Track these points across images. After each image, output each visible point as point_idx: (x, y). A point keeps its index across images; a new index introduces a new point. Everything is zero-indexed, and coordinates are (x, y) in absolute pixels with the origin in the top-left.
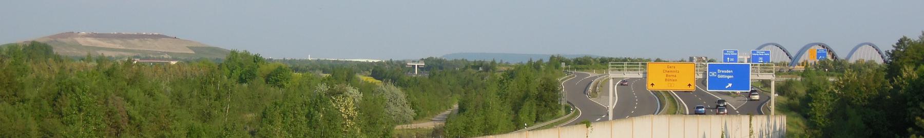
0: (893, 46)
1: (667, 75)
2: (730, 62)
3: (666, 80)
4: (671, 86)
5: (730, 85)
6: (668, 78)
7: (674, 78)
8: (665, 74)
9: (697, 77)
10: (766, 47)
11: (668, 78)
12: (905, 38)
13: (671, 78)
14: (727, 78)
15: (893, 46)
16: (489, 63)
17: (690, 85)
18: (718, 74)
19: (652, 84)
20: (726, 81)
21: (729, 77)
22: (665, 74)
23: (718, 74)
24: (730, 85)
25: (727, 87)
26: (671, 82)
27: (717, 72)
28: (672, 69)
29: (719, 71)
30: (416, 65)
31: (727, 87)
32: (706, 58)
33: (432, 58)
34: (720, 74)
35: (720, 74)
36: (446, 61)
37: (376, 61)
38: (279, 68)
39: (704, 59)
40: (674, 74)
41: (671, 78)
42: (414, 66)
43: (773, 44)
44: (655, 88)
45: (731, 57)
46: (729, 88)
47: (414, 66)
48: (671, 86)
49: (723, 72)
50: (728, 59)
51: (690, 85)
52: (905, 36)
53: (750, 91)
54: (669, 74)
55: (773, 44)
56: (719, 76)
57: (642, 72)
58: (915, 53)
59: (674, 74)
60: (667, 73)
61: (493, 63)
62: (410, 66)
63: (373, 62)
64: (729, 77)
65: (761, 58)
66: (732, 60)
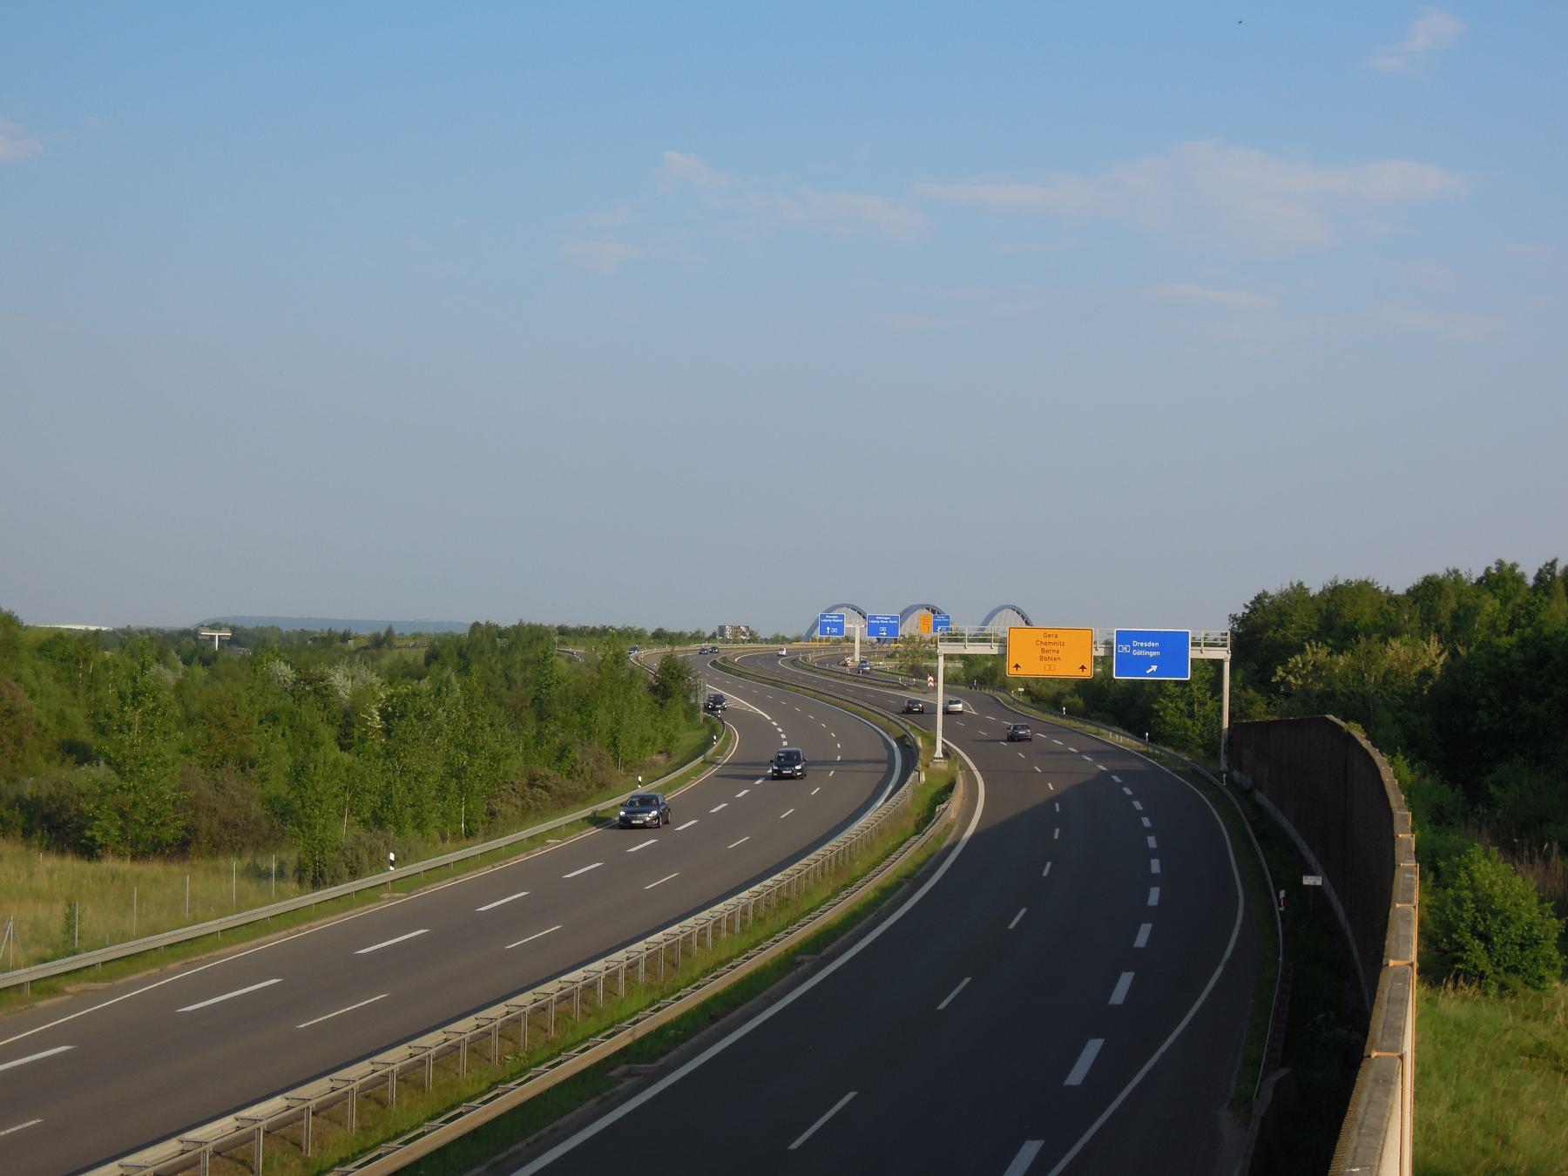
0: (1246, 606)
1: (1043, 650)
2: (831, 634)
3: (1041, 658)
4: (1050, 669)
5: (1154, 668)
6: (1044, 655)
7: (1056, 655)
8: (1040, 647)
9: (1096, 653)
10: (839, 609)
11: (1044, 655)
12: (1265, 594)
13: (1050, 655)
14: (1148, 656)
15: (1246, 606)
16: (466, 631)
17: (1083, 668)
18: (1132, 648)
19: (1017, 666)
20: (1148, 661)
21: (1152, 654)
22: (1040, 647)
23: (1132, 648)
24: (1154, 668)
25: (1148, 672)
26: (1050, 662)
27: (1131, 645)
28: (1053, 640)
29: (1135, 643)
30: (217, 635)
31: (1148, 672)
32: (747, 628)
33: (1364, 589)
34: (1139, 648)
35: (1139, 648)
36: (245, 630)
37: (104, 629)
38: (56, 636)
39: (743, 628)
40: (1055, 648)
41: (1050, 655)
42: (213, 638)
43: (848, 606)
44: (1021, 672)
45: (832, 625)
46: (1152, 674)
47: (213, 638)
48: (1050, 669)
49: (1142, 644)
50: (828, 628)
51: (1017, 666)
52: (1266, 590)
53: (1115, 677)
54: (1046, 648)
55: (848, 606)
56: (1135, 653)
57: (997, 644)
58: (1306, 619)
59: (1055, 648)
60: (1044, 647)
61: (389, 632)
62: (206, 638)
63: (98, 631)
64: (1152, 654)
65: (883, 629)
66: (835, 630)
